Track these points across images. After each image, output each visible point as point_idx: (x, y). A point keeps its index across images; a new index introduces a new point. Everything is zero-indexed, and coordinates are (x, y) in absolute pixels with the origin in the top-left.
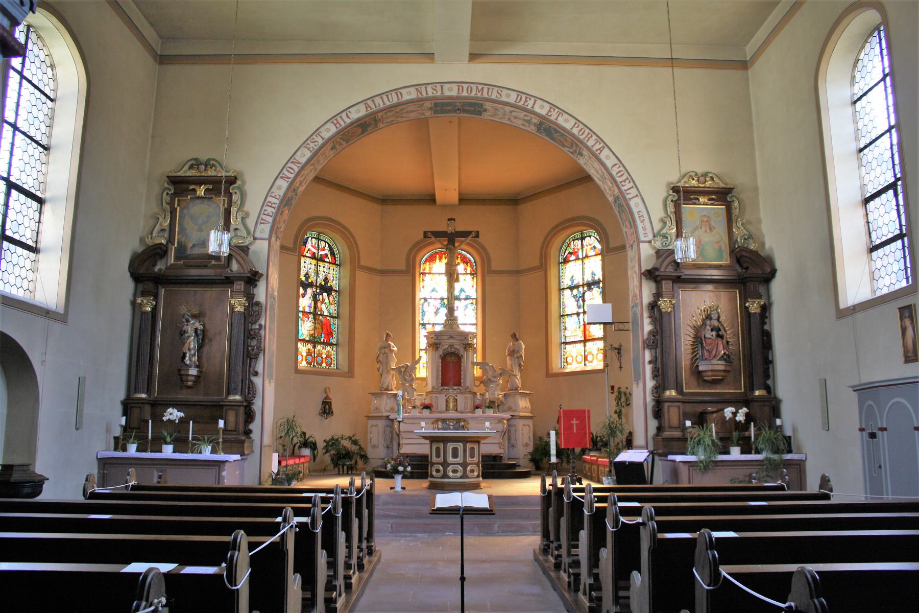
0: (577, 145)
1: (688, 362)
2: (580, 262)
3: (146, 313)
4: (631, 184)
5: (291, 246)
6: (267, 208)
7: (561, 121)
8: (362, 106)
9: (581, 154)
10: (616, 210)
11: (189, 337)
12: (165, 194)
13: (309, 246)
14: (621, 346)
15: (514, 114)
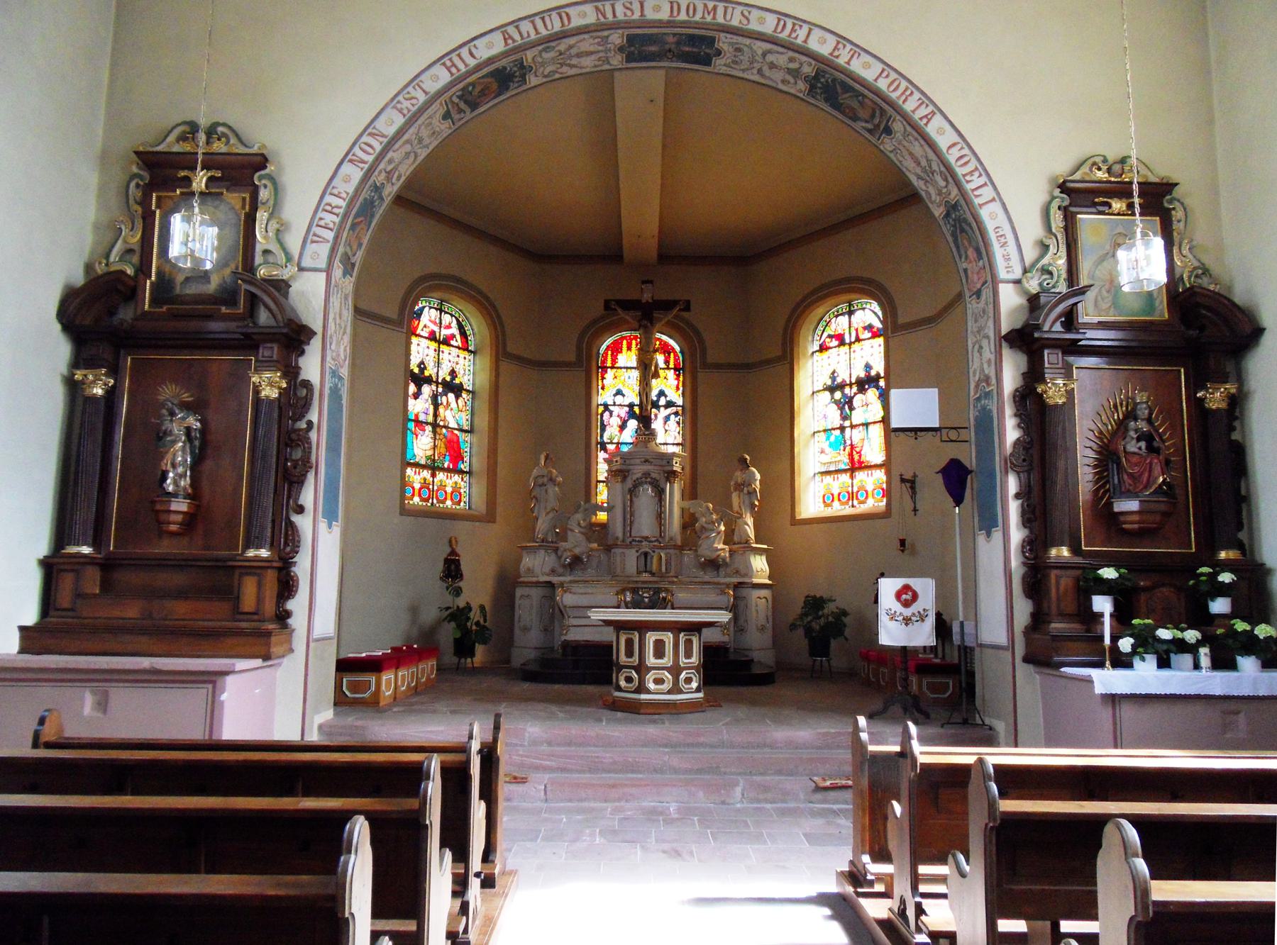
0: (883, 111)
1: (1089, 497)
2: (847, 347)
3: (94, 398)
4: (984, 179)
5: (395, 316)
6: (324, 215)
7: (857, 67)
8: (497, 38)
9: (888, 131)
10: (946, 230)
11: (174, 442)
12: (133, 184)
13: (425, 319)
14: (915, 476)
15: (770, 58)
